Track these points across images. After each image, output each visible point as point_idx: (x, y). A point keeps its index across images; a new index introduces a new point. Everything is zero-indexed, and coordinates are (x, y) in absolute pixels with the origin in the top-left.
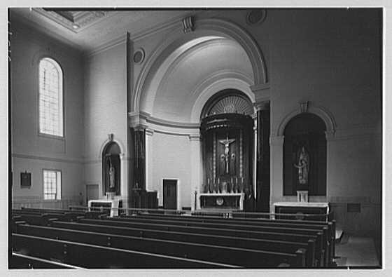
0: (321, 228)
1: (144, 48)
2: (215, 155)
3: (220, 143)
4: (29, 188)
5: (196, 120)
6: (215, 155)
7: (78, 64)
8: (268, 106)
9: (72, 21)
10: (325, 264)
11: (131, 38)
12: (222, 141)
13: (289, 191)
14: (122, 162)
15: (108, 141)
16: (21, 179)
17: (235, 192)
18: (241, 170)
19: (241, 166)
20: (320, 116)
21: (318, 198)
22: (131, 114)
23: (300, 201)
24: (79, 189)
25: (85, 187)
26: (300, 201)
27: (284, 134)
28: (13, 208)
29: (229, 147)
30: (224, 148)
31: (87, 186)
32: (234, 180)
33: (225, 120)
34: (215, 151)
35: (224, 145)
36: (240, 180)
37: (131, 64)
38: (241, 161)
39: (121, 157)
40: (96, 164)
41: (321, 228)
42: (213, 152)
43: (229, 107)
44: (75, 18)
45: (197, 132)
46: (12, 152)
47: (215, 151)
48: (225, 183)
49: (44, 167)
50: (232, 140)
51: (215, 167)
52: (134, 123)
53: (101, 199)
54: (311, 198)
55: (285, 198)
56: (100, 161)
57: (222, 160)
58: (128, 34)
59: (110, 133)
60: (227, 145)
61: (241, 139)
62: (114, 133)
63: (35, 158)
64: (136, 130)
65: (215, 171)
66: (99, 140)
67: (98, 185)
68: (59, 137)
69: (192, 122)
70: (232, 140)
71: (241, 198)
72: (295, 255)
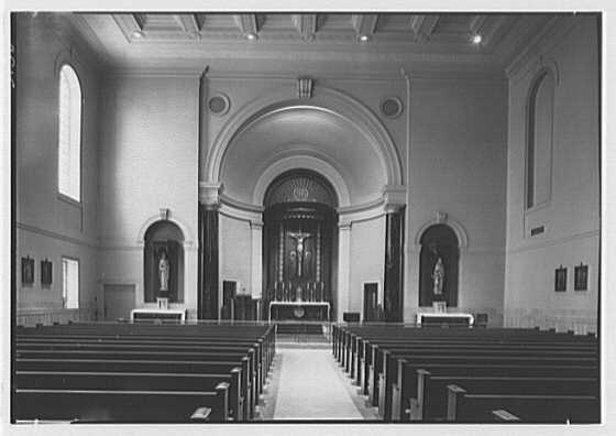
0: (246, 352)
1: (229, 95)
2: (282, 251)
3: (291, 237)
4: (31, 286)
5: (258, 202)
6: (282, 251)
7: (106, 83)
8: (403, 209)
9: (142, 27)
10: (593, 356)
11: (207, 75)
12: (293, 235)
13: (426, 299)
14: (186, 254)
15: (160, 218)
16: (29, 272)
17: (304, 300)
18: (318, 273)
19: (318, 268)
20: (457, 233)
21: (453, 309)
22: (203, 184)
23: (437, 311)
24: (103, 289)
25: (102, 289)
26: (437, 311)
27: (421, 242)
28: (18, 324)
29: (303, 243)
30: (296, 243)
31: (105, 286)
32: (311, 285)
33: (313, 210)
34: (282, 246)
35: (295, 239)
36: (319, 285)
37: (205, 112)
38: (318, 262)
39: (186, 246)
40: (130, 252)
41: (246, 352)
42: (279, 248)
43: (301, 193)
44: (146, 25)
45: (258, 218)
46: (18, 220)
47: (282, 246)
48: (299, 290)
49: (64, 252)
50: (308, 235)
51: (281, 267)
52: (208, 198)
53: (143, 308)
54: (172, 305)
55: (421, 309)
56: (138, 248)
57: (293, 259)
58: (207, 69)
59: (166, 207)
60: (301, 240)
61: (319, 235)
62: (170, 208)
63: (44, 233)
64: (210, 209)
65: (281, 273)
66: (136, 210)
67: (134, 286)
68: (73, 200)
69: (255, 203)
70: (308, 235)
71: (426, 315)
72: (215, 393)
